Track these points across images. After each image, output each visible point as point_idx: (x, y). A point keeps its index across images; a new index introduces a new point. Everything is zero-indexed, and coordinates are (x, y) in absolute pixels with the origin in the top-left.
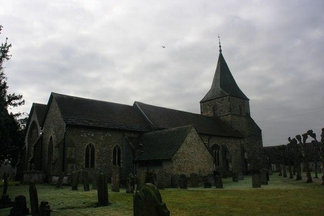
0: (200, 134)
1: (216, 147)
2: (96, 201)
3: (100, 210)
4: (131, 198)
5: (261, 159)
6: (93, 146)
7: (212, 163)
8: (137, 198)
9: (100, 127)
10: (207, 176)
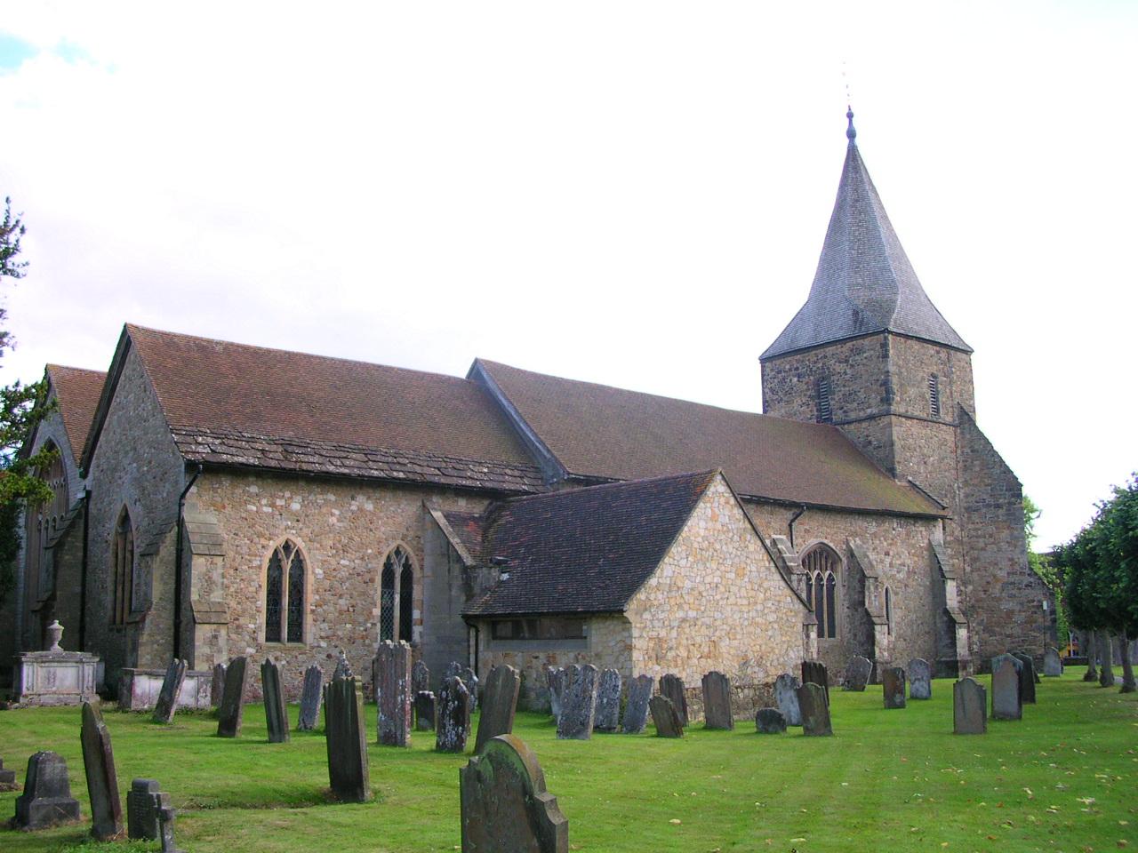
1: (820, 557)
3: (341, 813)
4: (451, 769)
8: (471, 778)
10: (774, 684)
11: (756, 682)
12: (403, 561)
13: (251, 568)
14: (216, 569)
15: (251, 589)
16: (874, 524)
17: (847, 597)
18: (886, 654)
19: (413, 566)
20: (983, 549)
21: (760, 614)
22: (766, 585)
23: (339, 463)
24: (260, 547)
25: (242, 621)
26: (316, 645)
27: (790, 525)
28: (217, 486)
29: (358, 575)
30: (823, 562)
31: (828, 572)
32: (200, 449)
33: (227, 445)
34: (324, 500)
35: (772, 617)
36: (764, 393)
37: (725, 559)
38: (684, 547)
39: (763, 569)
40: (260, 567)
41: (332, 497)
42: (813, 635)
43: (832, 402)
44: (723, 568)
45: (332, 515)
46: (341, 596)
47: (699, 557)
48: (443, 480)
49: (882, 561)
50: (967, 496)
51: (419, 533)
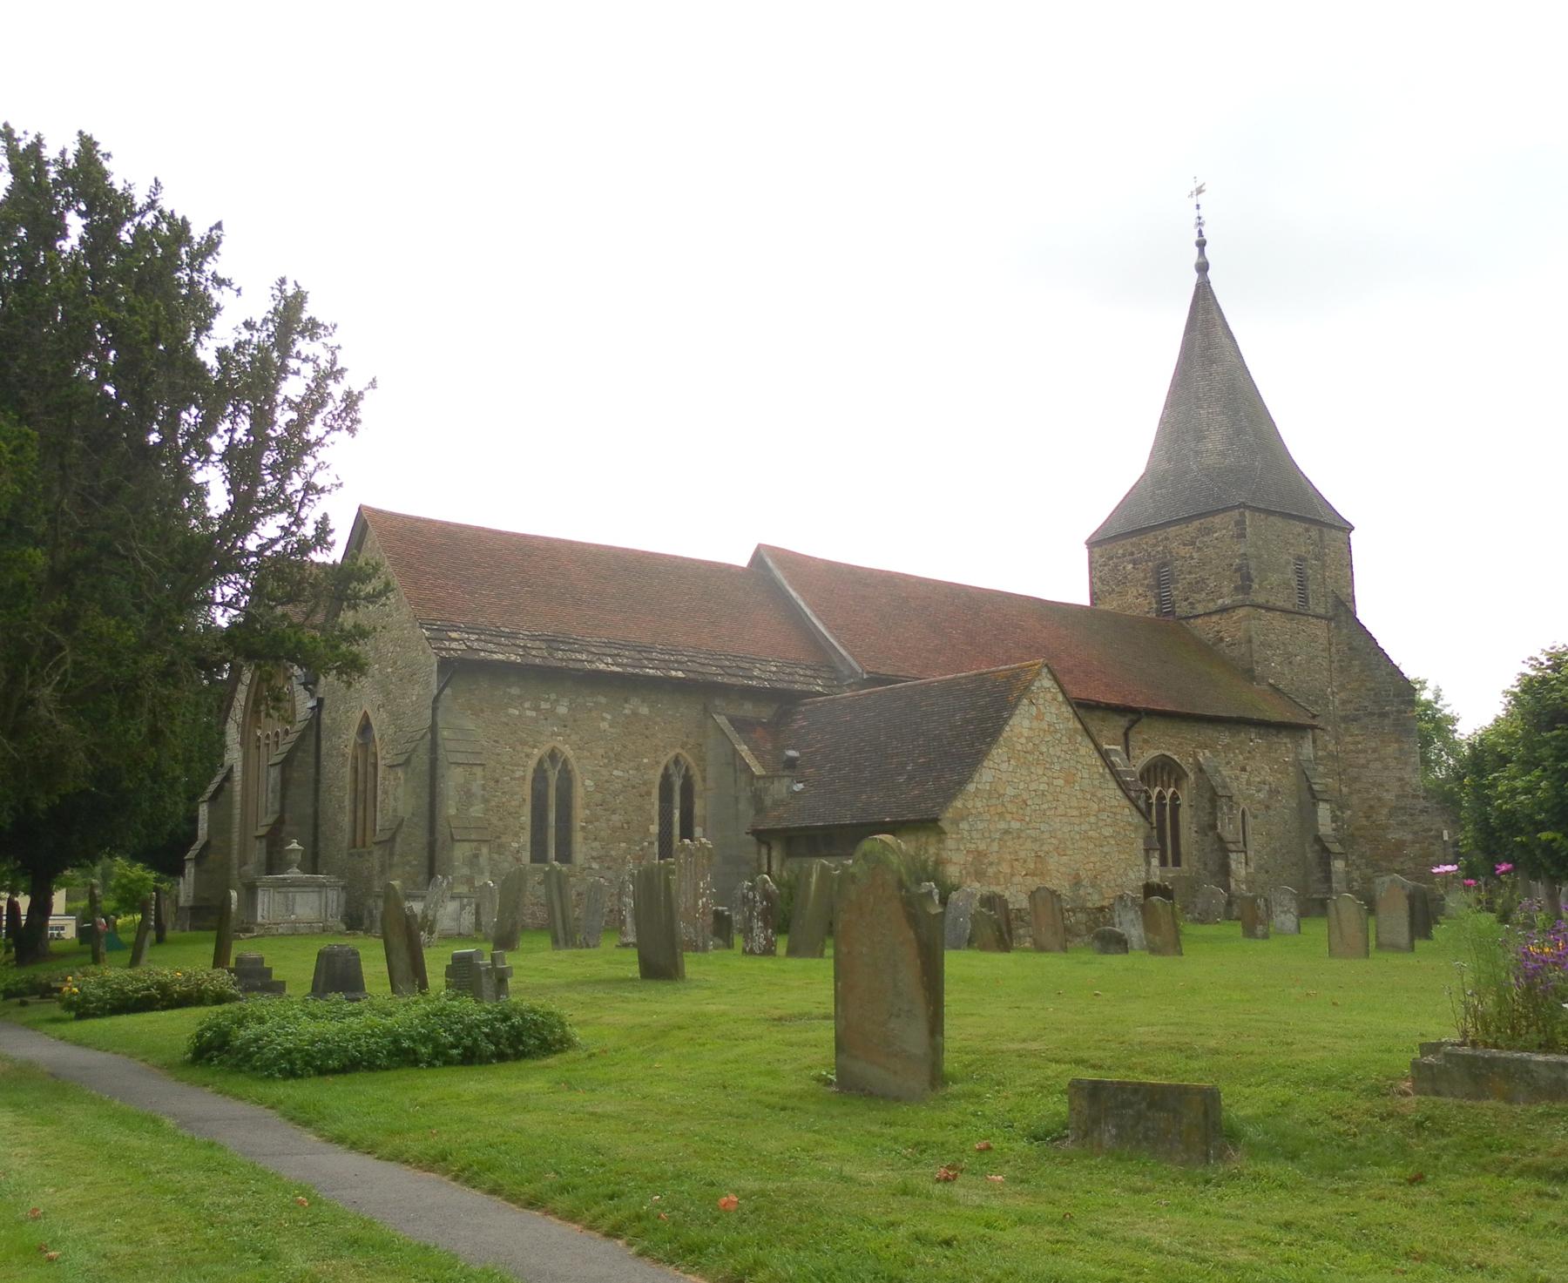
0: (1084, 708)
1: (1165, 770)
5: (1409, 837)
6: (565, 762)
7: (1140, 844)
9: (598, 672)
11: (1089, 905)
13: (515, 779)
15: (513, 803)
16: (1227, 734)
17: (1195, 820)
18: (1244, 887)
19: (694, 778)
20: (1363, 766)
21: (1094, 826)
22: (1100, 794)
23: (610, 661)
24: (523, 755)
25: (504, 839)
26: (587, 866)
27: (1126, 735)
28: (475, 687)
29: (634, 787)
31: (1172, 790)
32: (454, 645)
33: (485, 641)
35: (1107, 832)
36: (1091, 583)
38: (1005, 749)
40: (523, 778)
41: (603, 700)
42: (1155, 862)
45: (604, 719)
46: (614, 812)
47: (1022, 760)
49: (1237, 778)
50: (1343, 703)
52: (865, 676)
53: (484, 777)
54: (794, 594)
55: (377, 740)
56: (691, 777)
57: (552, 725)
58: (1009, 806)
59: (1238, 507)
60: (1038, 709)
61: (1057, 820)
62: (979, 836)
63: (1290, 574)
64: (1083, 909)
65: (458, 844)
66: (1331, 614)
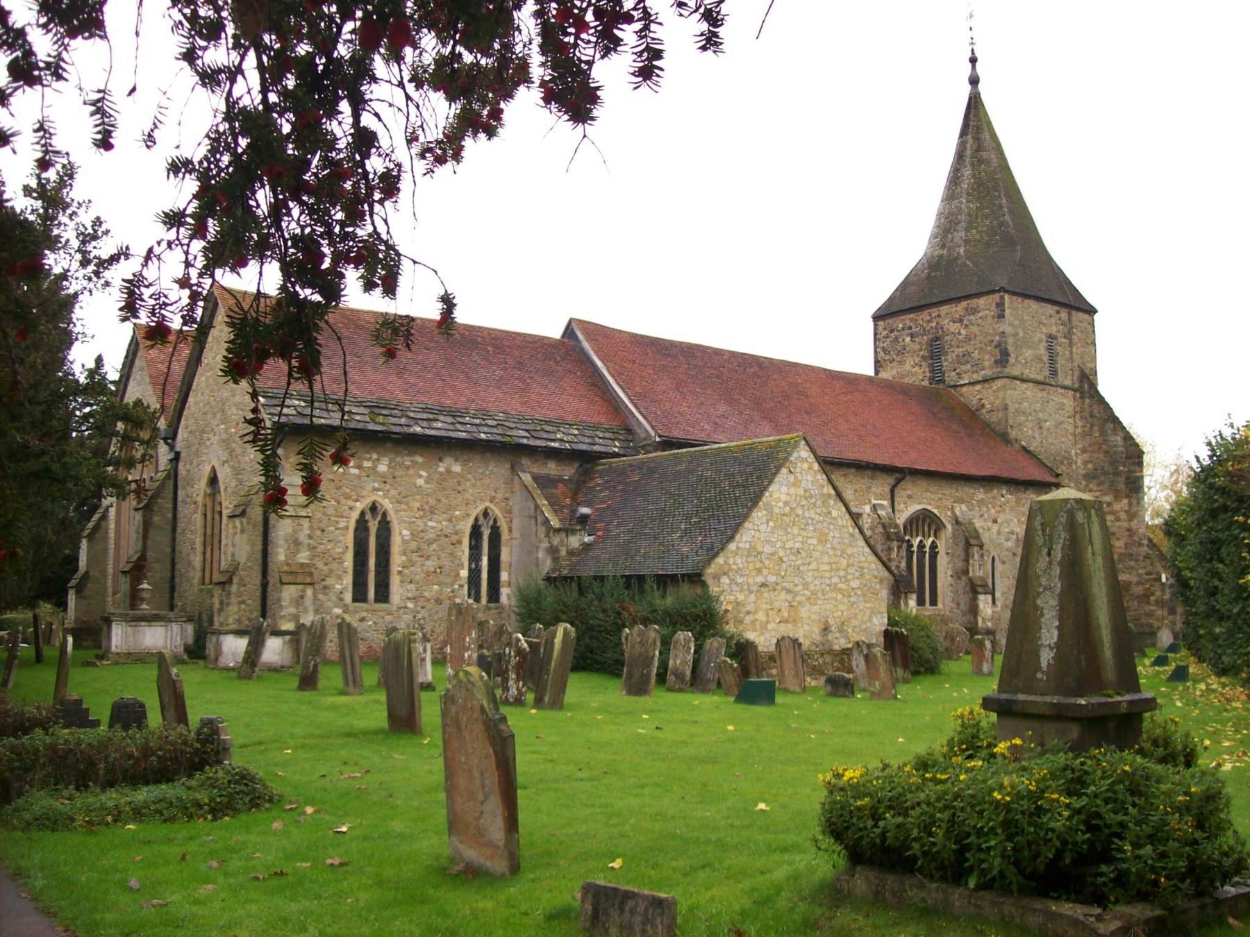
1: (925, 521)
2: (385, 724)
6: (384, 515)
9: (414, 435)
11: (836, 647)
12: (491, 523)
13: (339, 529)
14: (302, 530)
17: (950, 566)
24: (346, 508)
25: (329, 581)
27: (892, 491)
29: (446, 536)
30: (926, 529)
34: (412, 461)
37: (807, 524)
38: (765, 512)
39: (846, 536)
40: (347, 528)
41: (419, 459)
43: (945, 364)
44: (805, 533)
45: (420, 476)
46: (428, 558)
48: (532, 442)
49: (989, 529)
51: (507, 495)
52: (658, 439)
53: (311, 527)
54: (599, 363)
55: (222, 490)
56: (498, 528)
57: (374, 481)
58: (767, 562)
59: (999, 291)
60: (796, 478)
61: (810, 574)
62: (738, 589)
63: (1042, 351)
64: (831, 652)
65: (285, 587)
66: (1076, 386)
